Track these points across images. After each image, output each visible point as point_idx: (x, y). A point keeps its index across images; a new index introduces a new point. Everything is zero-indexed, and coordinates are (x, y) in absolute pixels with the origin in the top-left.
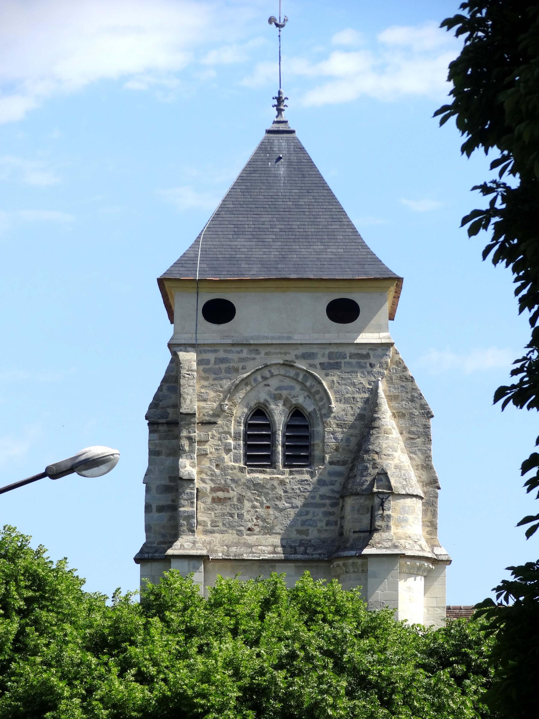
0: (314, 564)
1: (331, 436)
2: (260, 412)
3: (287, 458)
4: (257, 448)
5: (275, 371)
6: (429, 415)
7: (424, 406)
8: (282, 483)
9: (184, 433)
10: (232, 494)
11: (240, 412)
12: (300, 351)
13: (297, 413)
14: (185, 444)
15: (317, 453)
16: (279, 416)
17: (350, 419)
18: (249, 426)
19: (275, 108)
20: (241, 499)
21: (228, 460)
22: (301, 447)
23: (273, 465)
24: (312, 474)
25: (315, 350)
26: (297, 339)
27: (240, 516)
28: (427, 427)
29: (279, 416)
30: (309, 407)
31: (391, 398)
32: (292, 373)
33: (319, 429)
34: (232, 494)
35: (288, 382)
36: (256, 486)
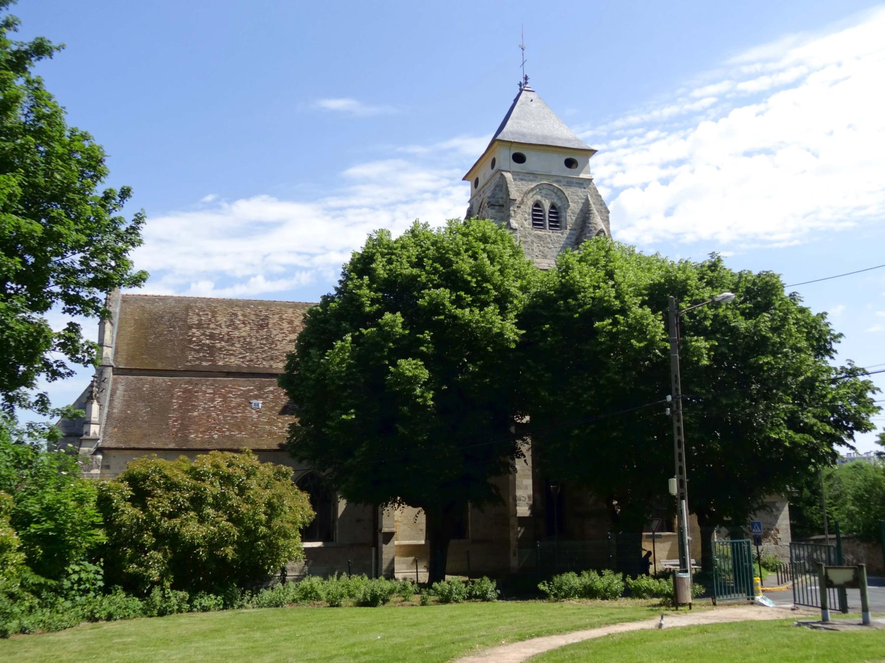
0: (634, 119)
1: (571, 217)
2: (537, 204)
3: (550, 226)
4: (537, 220)
5: (544, 186)
6: (608, 212)
7: (606, 208)
8: (550, 236)
9: (512, 208)
10: (528, 239)
11: (530, 203)
12: (555, 179)
13: (553, 206)
14: (512, 213)
15: (563, 224)
16: (547, 205)
17: (578, 211)
18: (534, 210)
19: (836, 333)
20: (532, 242)
21: (526, 224)
22: (556, 222)
23: (545, 228)
24: (562, 234)
25: (560, 179)
26: (553, 173)
27: (533, 250)
28: (608, 217)
29: (547, 205)
30: (559, 204)
31: (594, 203)
32: (552, 188)
33: (564, 214)
34: (528, 239)
35: (550, 192)
36: (539, 237)
